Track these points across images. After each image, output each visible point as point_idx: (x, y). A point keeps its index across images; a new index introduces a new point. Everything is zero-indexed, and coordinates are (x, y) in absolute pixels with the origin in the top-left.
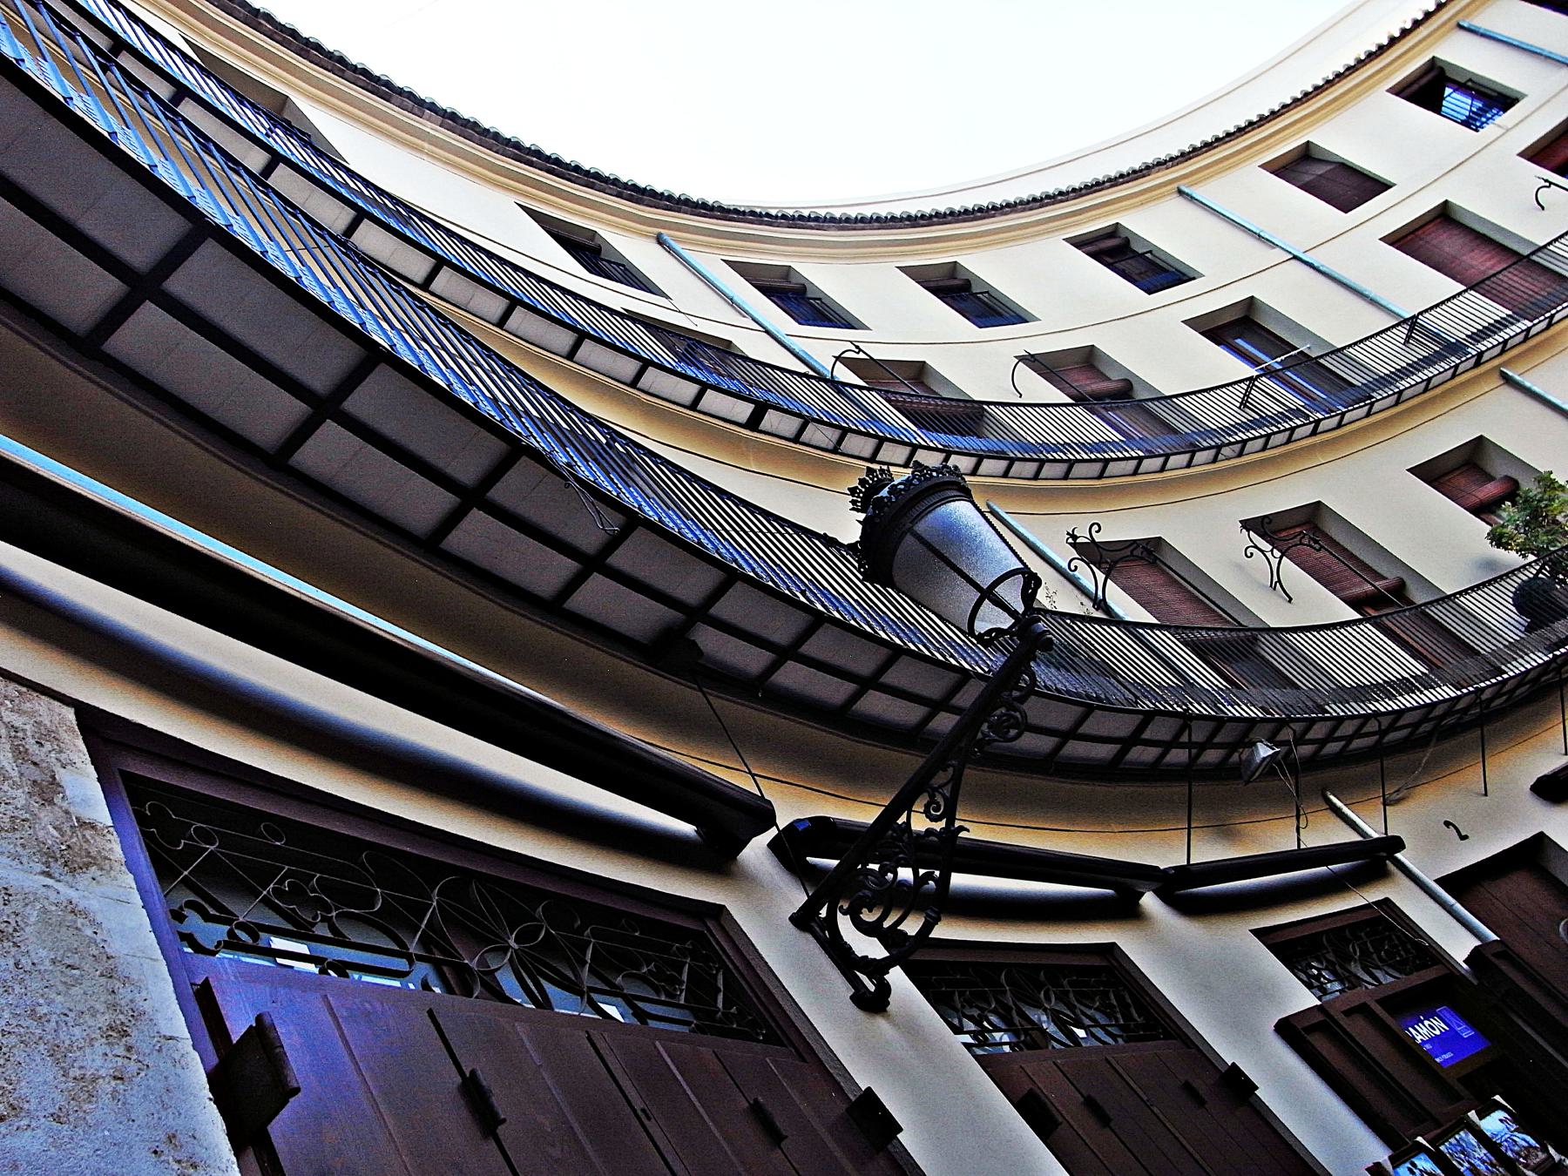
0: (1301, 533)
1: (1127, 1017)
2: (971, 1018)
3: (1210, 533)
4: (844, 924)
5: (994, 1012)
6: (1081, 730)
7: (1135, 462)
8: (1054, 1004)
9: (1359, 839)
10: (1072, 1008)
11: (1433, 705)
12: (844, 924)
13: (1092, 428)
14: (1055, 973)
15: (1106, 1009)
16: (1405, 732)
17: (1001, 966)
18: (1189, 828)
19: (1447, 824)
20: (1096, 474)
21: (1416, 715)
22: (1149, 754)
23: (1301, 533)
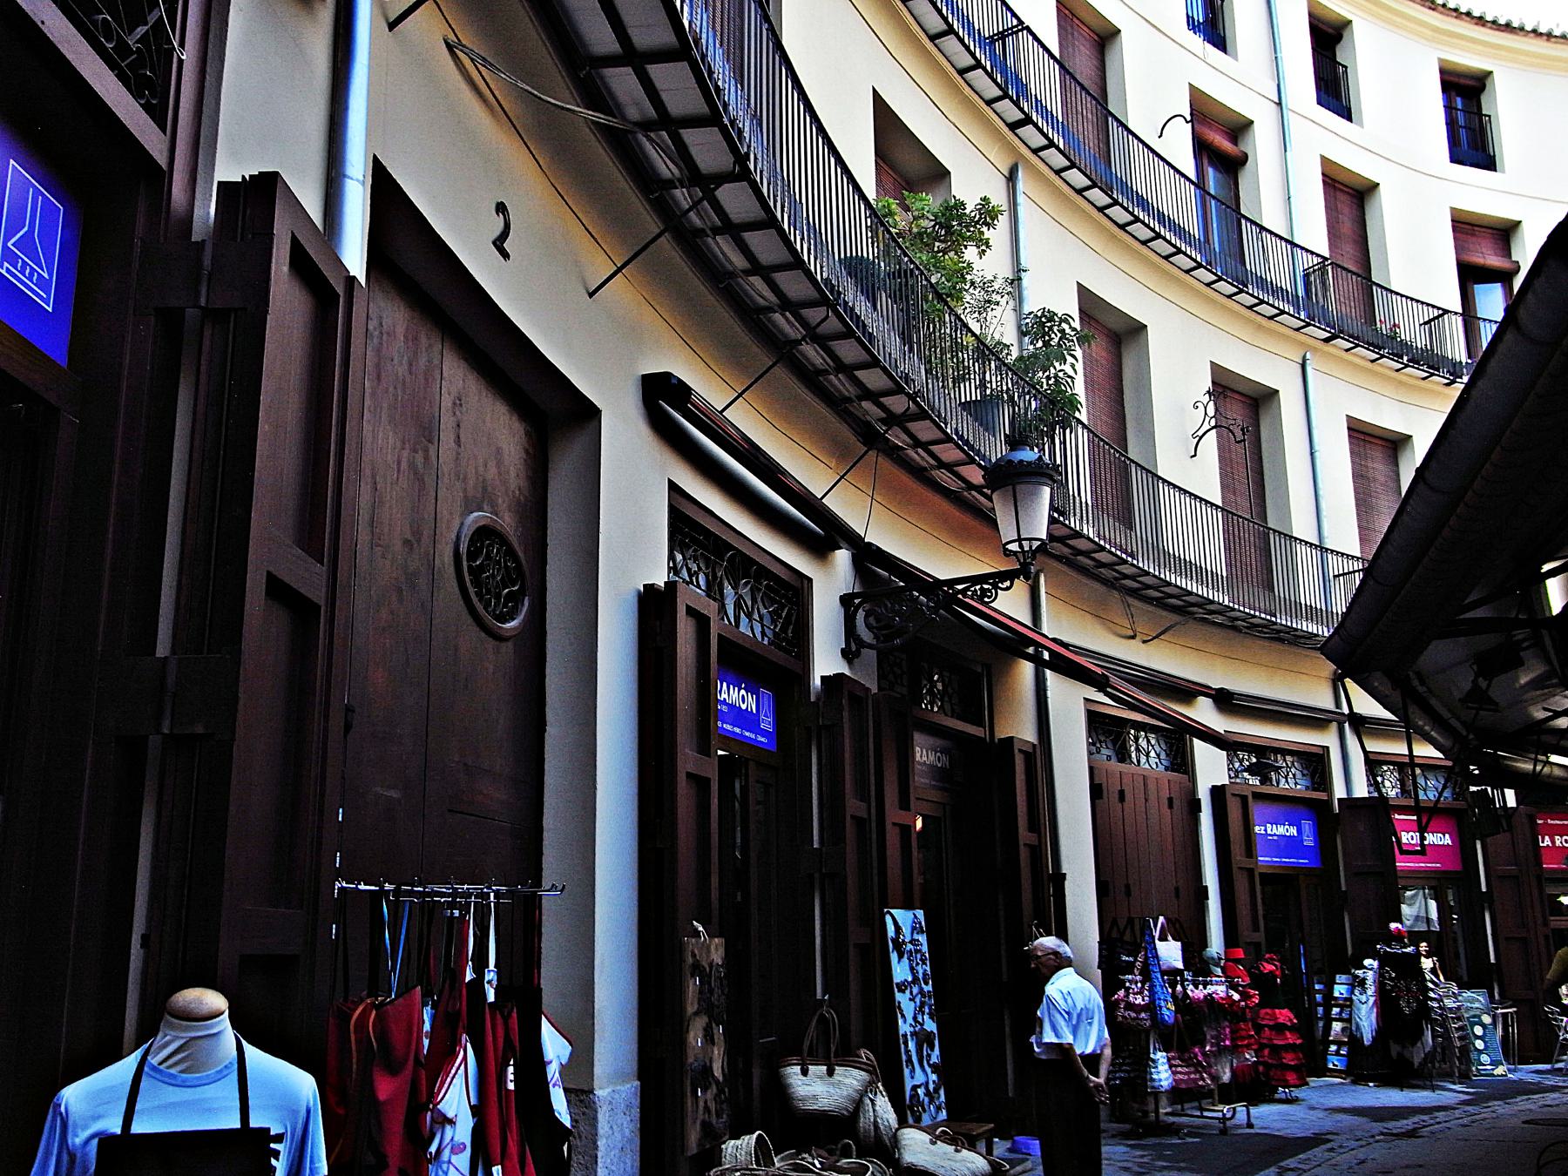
0: (1242, 407)
1: (784, 629)
2: (689, 570)
3: (1186, 348)
4: (861, 615)
5: (707, 575)
6: (858, 373)
7: (1045, 142)
8: (745, 591)
9: (1028, 621)
10: (754, 600)
11: (1169, 584)
12: (861, 615)
13: (1044, 82)
14: (763, 572)
15: (775, 616)
16: (1136, 585)
17: (731, 547)
18: (740, 395)
19: (501, 208)
20: (1034, 146)
21: (1176, 591)
22: (848, 389)
23: (1242, 407)
